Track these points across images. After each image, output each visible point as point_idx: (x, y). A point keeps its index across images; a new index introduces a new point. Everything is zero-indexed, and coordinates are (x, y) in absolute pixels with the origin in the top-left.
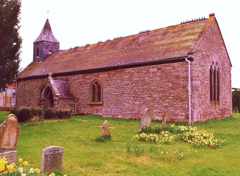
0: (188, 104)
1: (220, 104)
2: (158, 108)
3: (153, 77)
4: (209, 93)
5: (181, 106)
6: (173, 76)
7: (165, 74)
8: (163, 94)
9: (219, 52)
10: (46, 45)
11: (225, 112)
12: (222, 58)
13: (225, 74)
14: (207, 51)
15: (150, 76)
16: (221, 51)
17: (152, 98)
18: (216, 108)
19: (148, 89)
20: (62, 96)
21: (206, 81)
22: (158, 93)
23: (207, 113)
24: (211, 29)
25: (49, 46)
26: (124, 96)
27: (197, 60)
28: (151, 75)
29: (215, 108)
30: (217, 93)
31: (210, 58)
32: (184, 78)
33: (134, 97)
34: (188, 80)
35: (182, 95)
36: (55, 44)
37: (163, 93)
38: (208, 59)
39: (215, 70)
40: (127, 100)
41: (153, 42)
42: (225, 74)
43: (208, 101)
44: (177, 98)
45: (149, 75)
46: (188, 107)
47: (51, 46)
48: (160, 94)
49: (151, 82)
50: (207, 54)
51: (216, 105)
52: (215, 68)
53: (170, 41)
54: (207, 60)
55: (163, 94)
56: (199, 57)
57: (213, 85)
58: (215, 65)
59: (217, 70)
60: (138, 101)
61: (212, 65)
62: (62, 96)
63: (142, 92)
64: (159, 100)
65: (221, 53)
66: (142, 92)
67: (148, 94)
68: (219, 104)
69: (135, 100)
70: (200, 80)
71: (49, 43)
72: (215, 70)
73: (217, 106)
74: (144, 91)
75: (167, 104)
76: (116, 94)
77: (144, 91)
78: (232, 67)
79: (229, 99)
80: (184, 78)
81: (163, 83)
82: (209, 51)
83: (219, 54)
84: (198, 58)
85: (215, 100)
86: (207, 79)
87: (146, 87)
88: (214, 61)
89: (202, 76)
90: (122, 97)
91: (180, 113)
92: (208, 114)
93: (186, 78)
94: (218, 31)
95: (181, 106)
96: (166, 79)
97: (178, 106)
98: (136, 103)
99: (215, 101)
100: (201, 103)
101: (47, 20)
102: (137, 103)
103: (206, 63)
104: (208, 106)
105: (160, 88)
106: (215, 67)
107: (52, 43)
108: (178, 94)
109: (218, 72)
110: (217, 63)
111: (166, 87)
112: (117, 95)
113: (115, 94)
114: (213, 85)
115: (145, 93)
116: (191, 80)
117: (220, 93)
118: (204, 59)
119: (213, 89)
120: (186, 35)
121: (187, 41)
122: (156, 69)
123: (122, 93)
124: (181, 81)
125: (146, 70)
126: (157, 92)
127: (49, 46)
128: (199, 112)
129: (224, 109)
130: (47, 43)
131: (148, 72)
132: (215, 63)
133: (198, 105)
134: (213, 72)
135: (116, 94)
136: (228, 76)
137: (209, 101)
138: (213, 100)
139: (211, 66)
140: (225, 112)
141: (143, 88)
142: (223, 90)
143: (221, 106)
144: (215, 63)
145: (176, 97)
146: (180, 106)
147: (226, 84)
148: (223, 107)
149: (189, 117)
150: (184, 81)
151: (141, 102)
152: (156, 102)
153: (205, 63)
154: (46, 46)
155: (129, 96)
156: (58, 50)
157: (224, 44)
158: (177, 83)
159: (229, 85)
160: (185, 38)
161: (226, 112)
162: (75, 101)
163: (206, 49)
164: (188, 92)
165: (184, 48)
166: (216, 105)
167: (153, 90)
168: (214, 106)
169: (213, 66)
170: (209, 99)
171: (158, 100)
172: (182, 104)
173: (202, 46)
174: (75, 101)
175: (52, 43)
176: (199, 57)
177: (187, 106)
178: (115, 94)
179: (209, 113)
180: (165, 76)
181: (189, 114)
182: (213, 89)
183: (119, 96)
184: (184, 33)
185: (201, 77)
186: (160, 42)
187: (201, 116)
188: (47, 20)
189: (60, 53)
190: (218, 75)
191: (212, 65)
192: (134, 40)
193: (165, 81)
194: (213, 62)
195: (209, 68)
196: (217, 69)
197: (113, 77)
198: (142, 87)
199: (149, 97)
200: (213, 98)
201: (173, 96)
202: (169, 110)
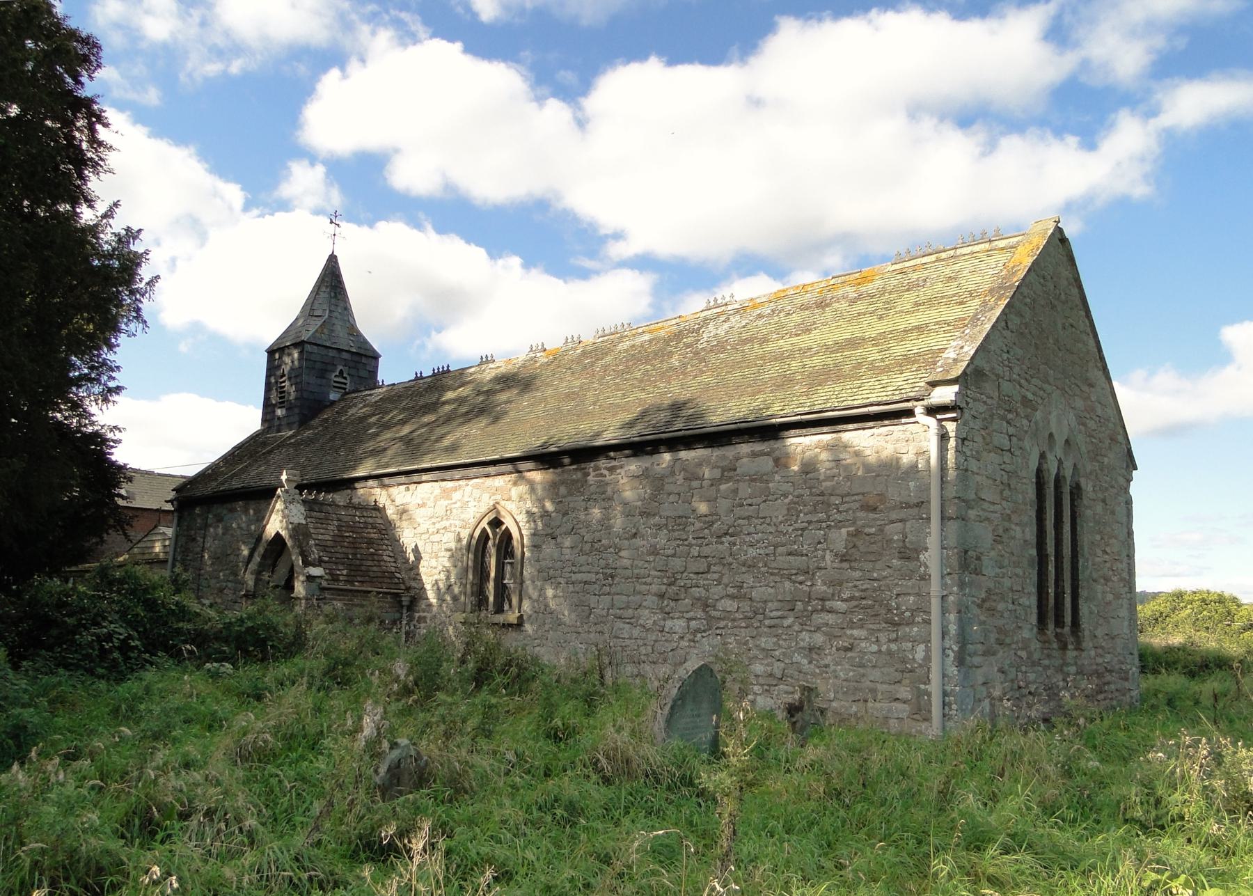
0: (927, 641)
1: (1084, 645)
2: (777, 653)
3: (755, 501)
4: (1034, 590)
5: (889, 651)
6: (848, 494)
7: (810, 488)
8: (801, 583)
9: (1078, 392)
10: (315, 361)
11: (1108, 683)
12: (1092, 424)
13: (1104, 501)
14: (1023, 381)
15: (741, 494)
16: (1085, 388)
17: (745, 606)
18: (1065, 664)
19: (730, 560)
20: (338, 580)
21: (1018, 528)
22: (778, 579)
23: (1025, 691)
24: (1042, 281)
25: (329, 367)
26: (614, 590)
27: (974, 417)
28: (745, 490)
29: (1062, 666)
30: (1068, 590)
31: (1038, 415)
32: (908, 506)
33: (662, 596)
34: (928, 519)
35: (898, 595)
36: (356, 358)
37: (801, 578)
38: (1027, 417)
39: (1058, 480)
40: (628, 607)
41: (765, 341)
42: (1104, 501)
43: (1028, 632)
44: (871, 607)
45: (736, 491)
46: (928, 658)
47: (340, 367)
48: (787, 584)
49: (745, 522)
50: (1024, 397)
51: (1064, 647)
52: (1058, 468)
53: (847, 332)
54: (1025, 422)
55: (801, 583)
56: (985, 403)
57: (1050, 549)
58: (1059, 451)
59: (1069, 479)
60: (677, 615)
61: (1046, 448)
62: (338, 580)
63: (698, 573)
64: (780, 613)
65: (1089, 398)
66: (698, 573)
67: (727, 586)
68: (1079, 648)
69: (667, 610)
70: (987, 519)
71: (332, 353)
72: (1058, 480)
73: (1071, 654)
74: (709, 567)
75: (819, 639)
76: (579, 576)
77: (709, 567)
78: (1136, 469)
79: (1126, 623)
80: (908, 506)
81: (803, 529)
82: (1034, 381)
83: (1079, 403)
84: (982, 408)
85: (1059, 622)
86: (1025, 519)
87: (720, 546)
88: (1054, 431)
89: (997, 499)
90: (608, 594)
91: (885, 687)
92: (1030, 693)
93: (919, 505)
94: (1075, 291)
95: (889, 651)
96: (815, 511)
97: (874, 648)
98: (669, 623)
99: (1063, 627)
100: (993, 637)
101: (332, 260)
102: (678, 625)
103: (1019, 440)
104: (1030, 654)
105: (790, 554)
106: (1060, 462)
107: (345, 355)
108: (875, 590)
109: (1076, 491)
110: (1067, 442)
111: (816, 550)
112: (586, 583)
113: (574, 577)
114: (1050, 549)
115: (716, 576)
116: (942, 519)
117: (1083, 593)
118: (1010, 416)
119: (1051, 568)
120: (917, 304)
121: (921, 329)
122: (771, 463)
123: (606, 577)
124: (892, 522)
125: (722, 468)
126: (772, 574)
127: (329, 367)
128: (984, 683)
129: (1101, 669)
130: (324, 352)
131: (731, 474)
132: (1060, 441)
133: (979, 646)
134: (1052, 485)
135: (579, 576)
136: (1120, 510)
137: (1035, 630)
138: (1051, 626)
139: (1043, 456)
140: (1108, 683)
141: (706, 551)
142: (1095, 575)
143: (1090, 656)
144: (1060, 441)
145: (864, 602)
146: (884, 648)
147: (1108, 550)
148: (1100, 660)
149: (930, 711)
150: (908, 524)
151: (693, 623)
152: (767, 622)
153: (1014, 439)
154: (318, 366)
155: (639, 593)
156: (370, 379)
157: (1102, 359)
158: (873, 530)
159: (1124, 554)
160: (914, 321)
161: (1113, 687)
162: (402, 606)
163: (1017, 369)
164: (925, 578)
165: (906, 361)
166: (1064, 647)
167: (751, 566)
168: (1055, 653)
169: (1050, 457)
170: (1034, 619)
171: (772, 615)
172: (896, 640)
173: (999, 352)
174: (402, 606)
175: (345, 355)
176: (985, 403)
177: (921, 648)
178: (574, 577)
179: (1032, 688)
180: (811, 494)
181: (929, 695)
182: (1051, 568)
183: (591, 588)
184: (908, 300)
185: (998, 507)
186: (795, 340)
187: (992, 705)
188: (332, 260)
189: (371, 395)
190: (1072, 500)
191: (1046, 448)
192: (679, 336)
193: (810, 522)
194: (1051, 435)
195: (1034, 465)
196: (1068, 473)
197: (569, 498)
198: (700, 546)
199: (732, 597)
200: (1051, 614)
201: (851, 598)
202: (826, 666)
